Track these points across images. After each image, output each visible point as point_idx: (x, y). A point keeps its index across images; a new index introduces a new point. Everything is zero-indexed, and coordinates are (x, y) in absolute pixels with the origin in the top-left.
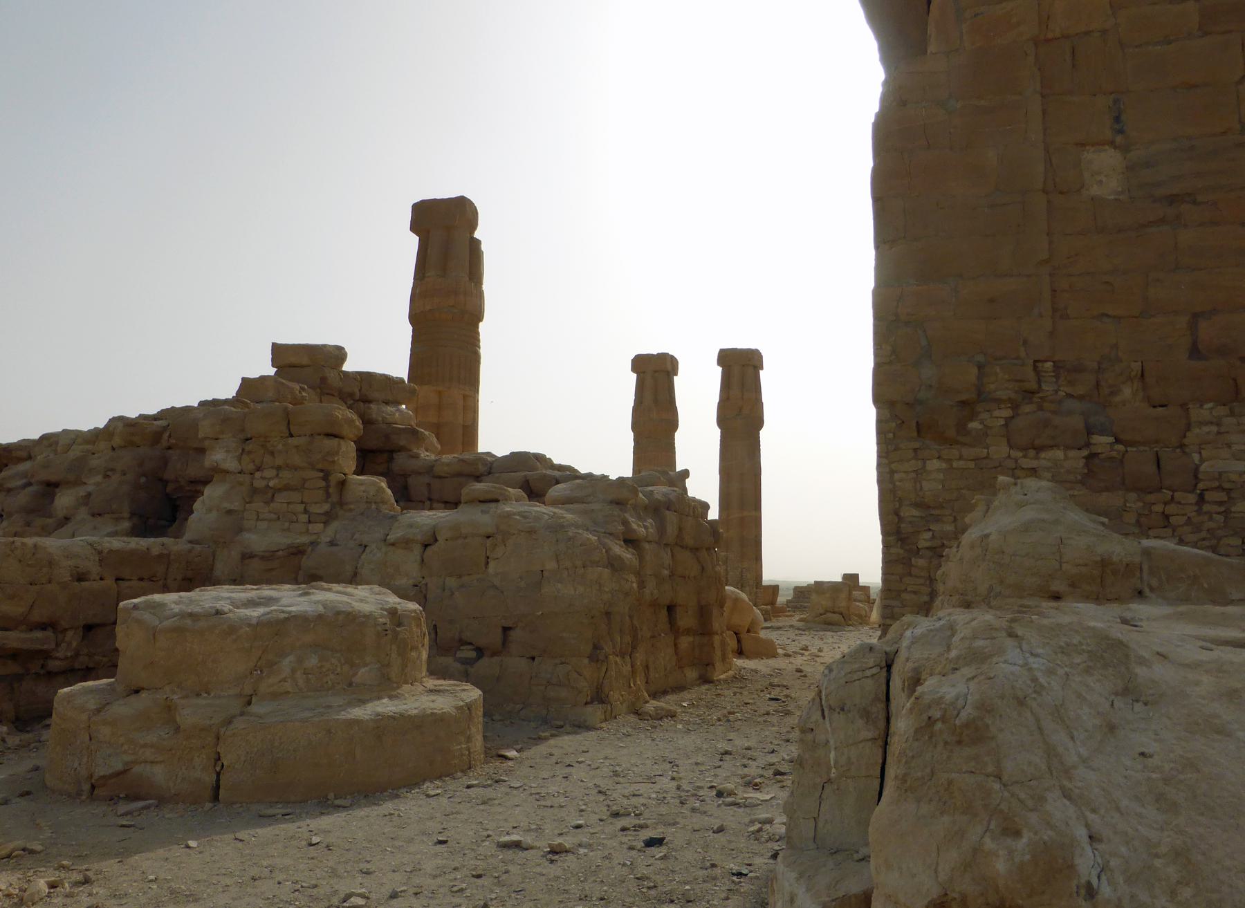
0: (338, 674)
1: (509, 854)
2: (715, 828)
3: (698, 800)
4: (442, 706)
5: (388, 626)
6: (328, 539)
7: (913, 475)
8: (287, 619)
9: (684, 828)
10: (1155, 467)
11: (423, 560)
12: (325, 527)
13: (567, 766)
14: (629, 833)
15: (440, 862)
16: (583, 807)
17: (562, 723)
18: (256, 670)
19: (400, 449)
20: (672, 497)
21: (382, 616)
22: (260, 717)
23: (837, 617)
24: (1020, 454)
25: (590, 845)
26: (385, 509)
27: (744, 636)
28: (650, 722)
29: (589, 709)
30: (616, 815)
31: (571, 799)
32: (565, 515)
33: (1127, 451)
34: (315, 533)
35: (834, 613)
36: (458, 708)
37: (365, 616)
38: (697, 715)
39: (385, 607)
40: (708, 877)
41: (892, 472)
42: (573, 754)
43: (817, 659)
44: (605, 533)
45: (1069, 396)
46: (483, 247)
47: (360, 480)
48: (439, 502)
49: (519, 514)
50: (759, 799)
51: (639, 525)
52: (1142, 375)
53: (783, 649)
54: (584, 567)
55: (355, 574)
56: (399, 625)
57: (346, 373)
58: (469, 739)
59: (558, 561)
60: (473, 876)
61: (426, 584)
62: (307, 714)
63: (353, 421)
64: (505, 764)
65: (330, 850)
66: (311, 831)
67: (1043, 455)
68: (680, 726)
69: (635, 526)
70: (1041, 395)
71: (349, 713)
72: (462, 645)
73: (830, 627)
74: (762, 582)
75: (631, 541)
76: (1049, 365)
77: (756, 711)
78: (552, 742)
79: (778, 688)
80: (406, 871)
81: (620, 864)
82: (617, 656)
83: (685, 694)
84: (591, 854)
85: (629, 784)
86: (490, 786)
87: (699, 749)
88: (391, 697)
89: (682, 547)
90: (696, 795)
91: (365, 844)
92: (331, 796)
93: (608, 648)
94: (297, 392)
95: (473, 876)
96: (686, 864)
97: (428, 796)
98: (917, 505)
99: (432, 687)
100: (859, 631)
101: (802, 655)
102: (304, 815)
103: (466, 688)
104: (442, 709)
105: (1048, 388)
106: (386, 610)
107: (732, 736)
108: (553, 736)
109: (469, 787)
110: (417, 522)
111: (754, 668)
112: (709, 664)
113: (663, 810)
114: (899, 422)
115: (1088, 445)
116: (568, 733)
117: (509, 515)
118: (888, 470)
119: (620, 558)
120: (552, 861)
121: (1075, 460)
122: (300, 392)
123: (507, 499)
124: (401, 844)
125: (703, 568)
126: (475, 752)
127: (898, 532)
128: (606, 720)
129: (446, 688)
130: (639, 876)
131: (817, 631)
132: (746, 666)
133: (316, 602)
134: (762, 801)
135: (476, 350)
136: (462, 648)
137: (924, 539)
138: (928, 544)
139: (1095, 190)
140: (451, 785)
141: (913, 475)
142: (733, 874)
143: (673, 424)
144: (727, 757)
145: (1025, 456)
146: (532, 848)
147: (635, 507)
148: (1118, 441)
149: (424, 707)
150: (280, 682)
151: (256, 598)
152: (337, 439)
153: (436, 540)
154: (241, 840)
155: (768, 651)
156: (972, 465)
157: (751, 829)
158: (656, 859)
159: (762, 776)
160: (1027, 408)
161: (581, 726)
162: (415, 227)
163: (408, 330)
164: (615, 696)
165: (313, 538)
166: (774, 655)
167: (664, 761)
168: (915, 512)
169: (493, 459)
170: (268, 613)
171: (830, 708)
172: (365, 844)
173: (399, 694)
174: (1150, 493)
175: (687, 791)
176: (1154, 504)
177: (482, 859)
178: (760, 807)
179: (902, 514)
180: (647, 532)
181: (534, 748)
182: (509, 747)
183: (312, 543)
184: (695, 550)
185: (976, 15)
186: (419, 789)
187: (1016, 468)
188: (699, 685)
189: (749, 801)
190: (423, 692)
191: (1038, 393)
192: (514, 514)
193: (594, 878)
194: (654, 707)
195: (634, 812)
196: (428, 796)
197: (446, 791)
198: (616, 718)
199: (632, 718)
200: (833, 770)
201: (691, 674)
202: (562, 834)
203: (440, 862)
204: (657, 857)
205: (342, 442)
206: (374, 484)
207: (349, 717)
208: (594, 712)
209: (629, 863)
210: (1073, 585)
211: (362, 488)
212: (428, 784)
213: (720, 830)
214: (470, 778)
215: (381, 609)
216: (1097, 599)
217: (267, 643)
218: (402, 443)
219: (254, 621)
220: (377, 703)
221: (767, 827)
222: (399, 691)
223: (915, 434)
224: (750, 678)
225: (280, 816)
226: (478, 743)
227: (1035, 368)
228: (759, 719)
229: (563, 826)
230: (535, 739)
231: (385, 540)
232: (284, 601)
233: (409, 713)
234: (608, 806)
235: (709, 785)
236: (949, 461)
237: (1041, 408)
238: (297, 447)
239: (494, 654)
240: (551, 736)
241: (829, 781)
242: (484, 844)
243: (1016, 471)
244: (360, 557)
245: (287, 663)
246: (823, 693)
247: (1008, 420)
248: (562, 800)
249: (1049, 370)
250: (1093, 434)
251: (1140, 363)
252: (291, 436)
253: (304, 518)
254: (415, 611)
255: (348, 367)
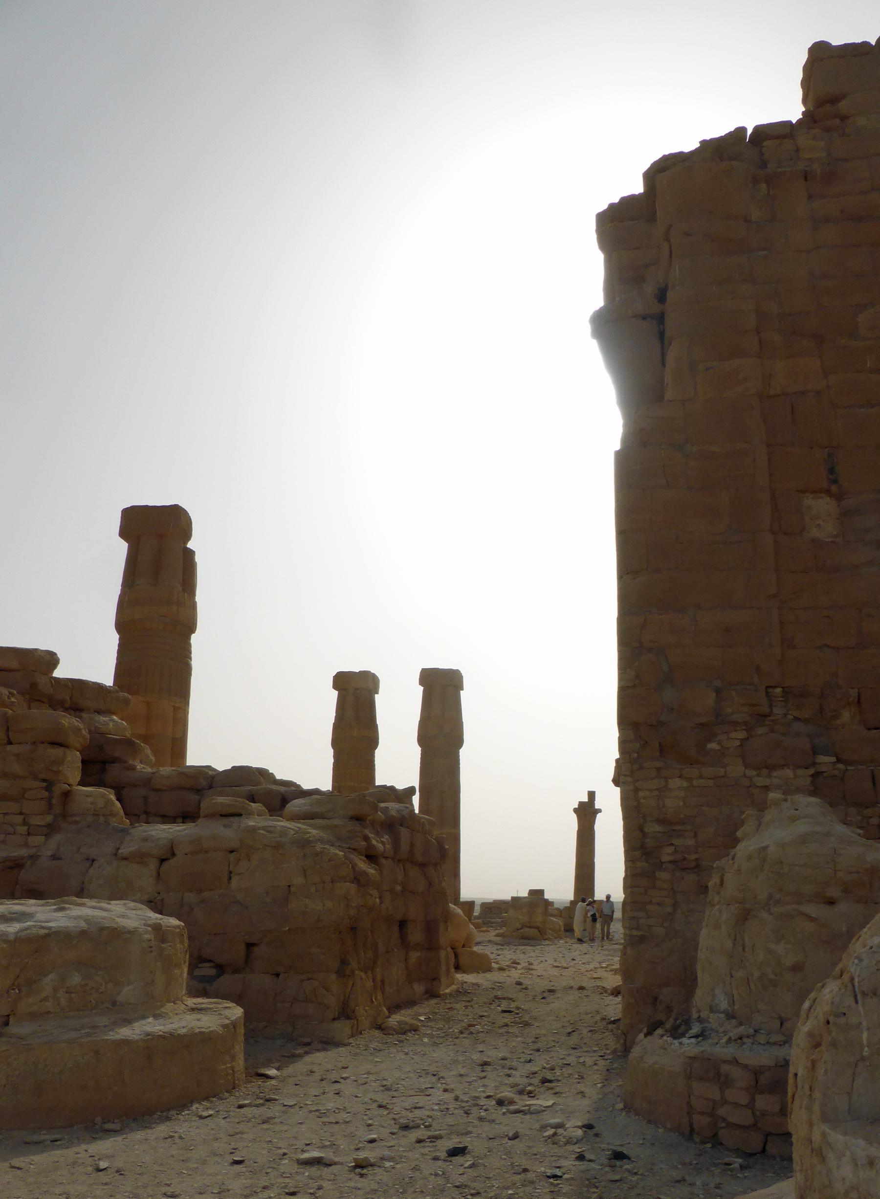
0: (102, 993)
1: (314, 1170)
2: (511, 1135)
3: (481, 1109)
4: (209, 1025)
5: (153, 943)
6: (50, 853)
7: (656, 793)
8: (48, 935)
9: (478, 1136)
10: (871, 784)
11: (159, 875)
12: (46, 839)
13: (333, 1083)
14: (427, 1144)
15: (244, 1181)
16: (370, 1122)
17: (309, 1040)
18: (14, 989)
19: (115, 760)
20: (405, 813)
21: (146, 932)
22: (21, 1038)
23: (533, 932)
24: (754, 773)
25: (393, 1158)
26: (114, 822)
27: (460, 950)
28: (396, 1036)
29: (337, 1025)
30: (406, 1128)
31: (354, 1114)
32: (309, 830)
33: (847, 770)
34: (36, 846)
35: (531, 927)
36: (224, 1026)
37: (129, 932)
38: (438, 1028)
39: (149, 922)
40: (525, 1181)
41: (637, 790)
42: (334, 1070)
43: (532, 972)
44: (349, 848)
45: (797, 719)
46: (198, 558)
47: (87, 791)
48: (156, 815)
49: (264, 828)
50: (541, 1106)
51: (377, 841)
52: (859, 701)
53: (497, 963)
54: (332, 882)
55: (82, 890)
56: (163, 940)
57: (58, 680)
58: (233, 1058)
59: (305, 876)
60: (287, 1193)
61: (162, 900)
62: (72, 1035)
63: (80, 730)
64: (268, 1083)
65: (121, 1174)
66: (93, 1156)
67: (775, 774)
68: (426, 1040)
69: (374, 842)
70: (772, 718)
71: (118, 1034)
72: (201, 962)
73: (527, 941)
74: (460, 898)
75: (371, 857)
76: (778, 690)
77: (494, 1023)
78: (308, 1059)
79: (504, 1001)
80: (212, 1193)
81: (431, 1174)
82: (361, 971)
83: (416, 1009)
84: (398, 1166)
85: (404, 1097)
86: (263, 1105)
87: (455, 1062)
88: (156, 1017)
89: (412, 863)
90: (478, 1105)
91: (156, 1168)
92: (98, 1120)
93: (354, 964)
94: (6, 697)
95: (287, 1193)
96: (498, 1171)
97: (201, 1117)
98: (660, 821)
99: (194, 1006)
100: (556, 945)
101: (516, 968)
102: (76, 1141)
103: (228, 1005)
104: (209, 1027)
105: (778, 711)
106: (149, 926)
107: (481, 1047)
108: (307, 1053)
109: (240, 1107)
110: (153, 835)
111: (474, 982)
112: (436, 979)
113: (450, 1120)
114: (642, 743)
115: (814, 764)
116: (318, 1050)
117: (254, 830)
118: (632, 787)
119: (366, 874)
120: (362, 1175)
121: (804, 777)
122: (9, 697)
123: (250, 814)
124: (195, 1166)
125: (430, 884)
126: (238, 1071)
127: (643, 847)
128: (352, 1036)
129: (209, 1006)
130: (457, 1184)
131: (516, 945)
132: (467, 980)
133: (76, 918)
134: (545, 1107)
135: (188, 661)
136: (200, 965)
137: (666, 853)
138: (671, 858)
139: (815, 533)
140: (221, 1106)
141: (656, 793)
142: (549, 1177)
143: (373, 742)
144: (488, 1068)
145: (758, 775)
146: (335, 1164)
147: (373, 823)
148: (839, 760)
149: (192, 1026)
150: (41, 1001)
151: (6, 913)
152: (62, 748)
153: (174, 855)
154: (19, 1168)
155: (482, 965)
156: (711, 783)
157: (546, 1134)
158: (465, 1168)
159: (530, 1085)
160: (760, 731)
161: (329, 1043)
162: (124, 533)
163: (113, 639)
164: (361, 1011)
165: (33, 851)
166: (489, 970)
167: (427, 1073)
168: (658, 828)
169: (215, 773)
170: (27, 929)
171: (864, 994)
172: (156, 1168)
173: (163, 1013)
174: (867, 808)
175: (467, 1102)
176: (871, 817)
177: (288, 1177)
178: (546, 1113)
179: (646, 830)
180: (384, 847)
181: (291, 1066)
182: (267, 1065)
183: (31, 857)
184: (422, 865)
185: (708, 369)
186: (189, 1110)
187: (750, 786)
188: (427, 999)
189: (533, 1108)
190: (185, 1011)
191: (770, 716)
192: (259, 829)
193: (412, 1189)
194: (397, 1022)
195: (423, 1124)
196: (201, 1117)
197: (218, 1111)
198: (361, 1033)
199: (377, 1033)
200: (866, 1049)
201: (419, 988)
202: (358, 1149)
203: (244, 1181)
204: (466, 1165)
205: (68, 752)
206: (103, 796)
207: (118, 1037)
208: (342, 1028)
209: (441, 1173)
210: (846, 891)
211: (90, 799)
212: (195, 1106)
213: (515, 1137)
214: (237, 1098)
215: (145, 925)
216: (866, 903)
217: (26, 960)
218: (117, 754)
219: (12, 937)
220: (143, 1022)
221: (560, 1131)
222: (163, 1010)
223: (658, 754)
224: (473, 991)
225: (49, 1142)
226: (240, 1063)
227: (767, 693)
228: (501, 1031)
229: (357, 1142)
230: (288, 1057)
231: (116, 854)
232: (40, 916)
233: (179, 1032)
234: (394, 1119)
235: (485, 1095)
236: (690, 779)
237: (772, 731)
238: (17, 755)
239: (236, 971)
240: (305, 1053)
241: (863, 1059)
242: (283, 1162)
243: (750, 789)
244: (87, 871)
245: (49, 980)
246: (856, 980)
247: (744, 741)
248: (344, 1115)
249: (779, 695)
250: (817, 754)
251: (856, 690)
252: (10, 743)
253: (23, 829)
254: (178, 927)
255: (59, 673)
